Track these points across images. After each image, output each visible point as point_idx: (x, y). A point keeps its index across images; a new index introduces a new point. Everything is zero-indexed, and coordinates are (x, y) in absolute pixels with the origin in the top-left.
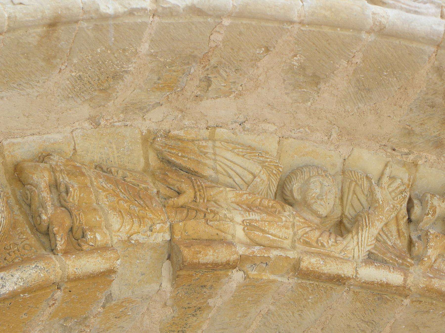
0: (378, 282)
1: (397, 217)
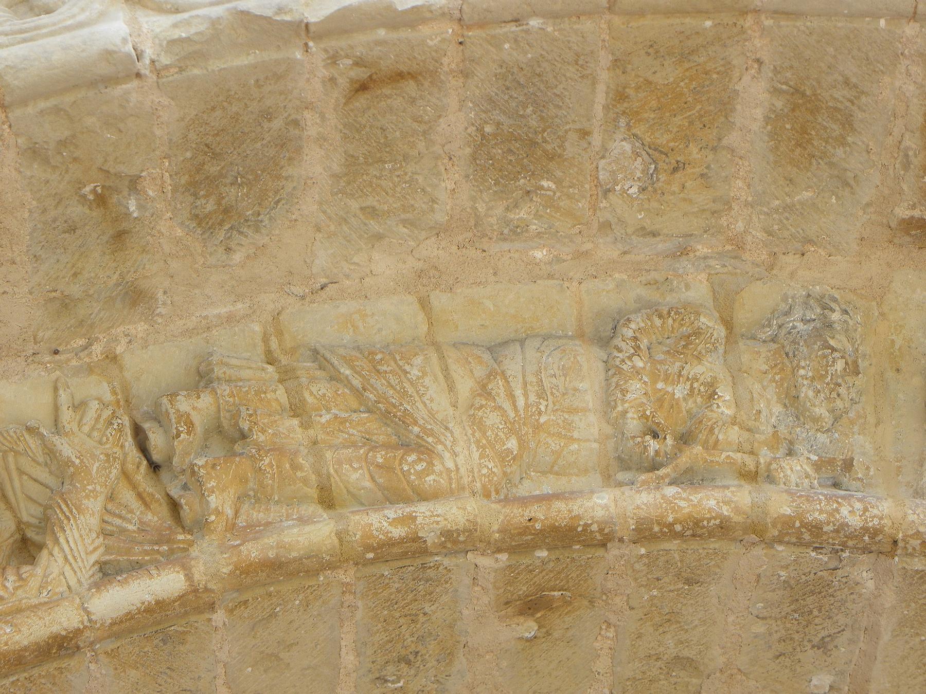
0: (139, 609)
1: (125, 474)
